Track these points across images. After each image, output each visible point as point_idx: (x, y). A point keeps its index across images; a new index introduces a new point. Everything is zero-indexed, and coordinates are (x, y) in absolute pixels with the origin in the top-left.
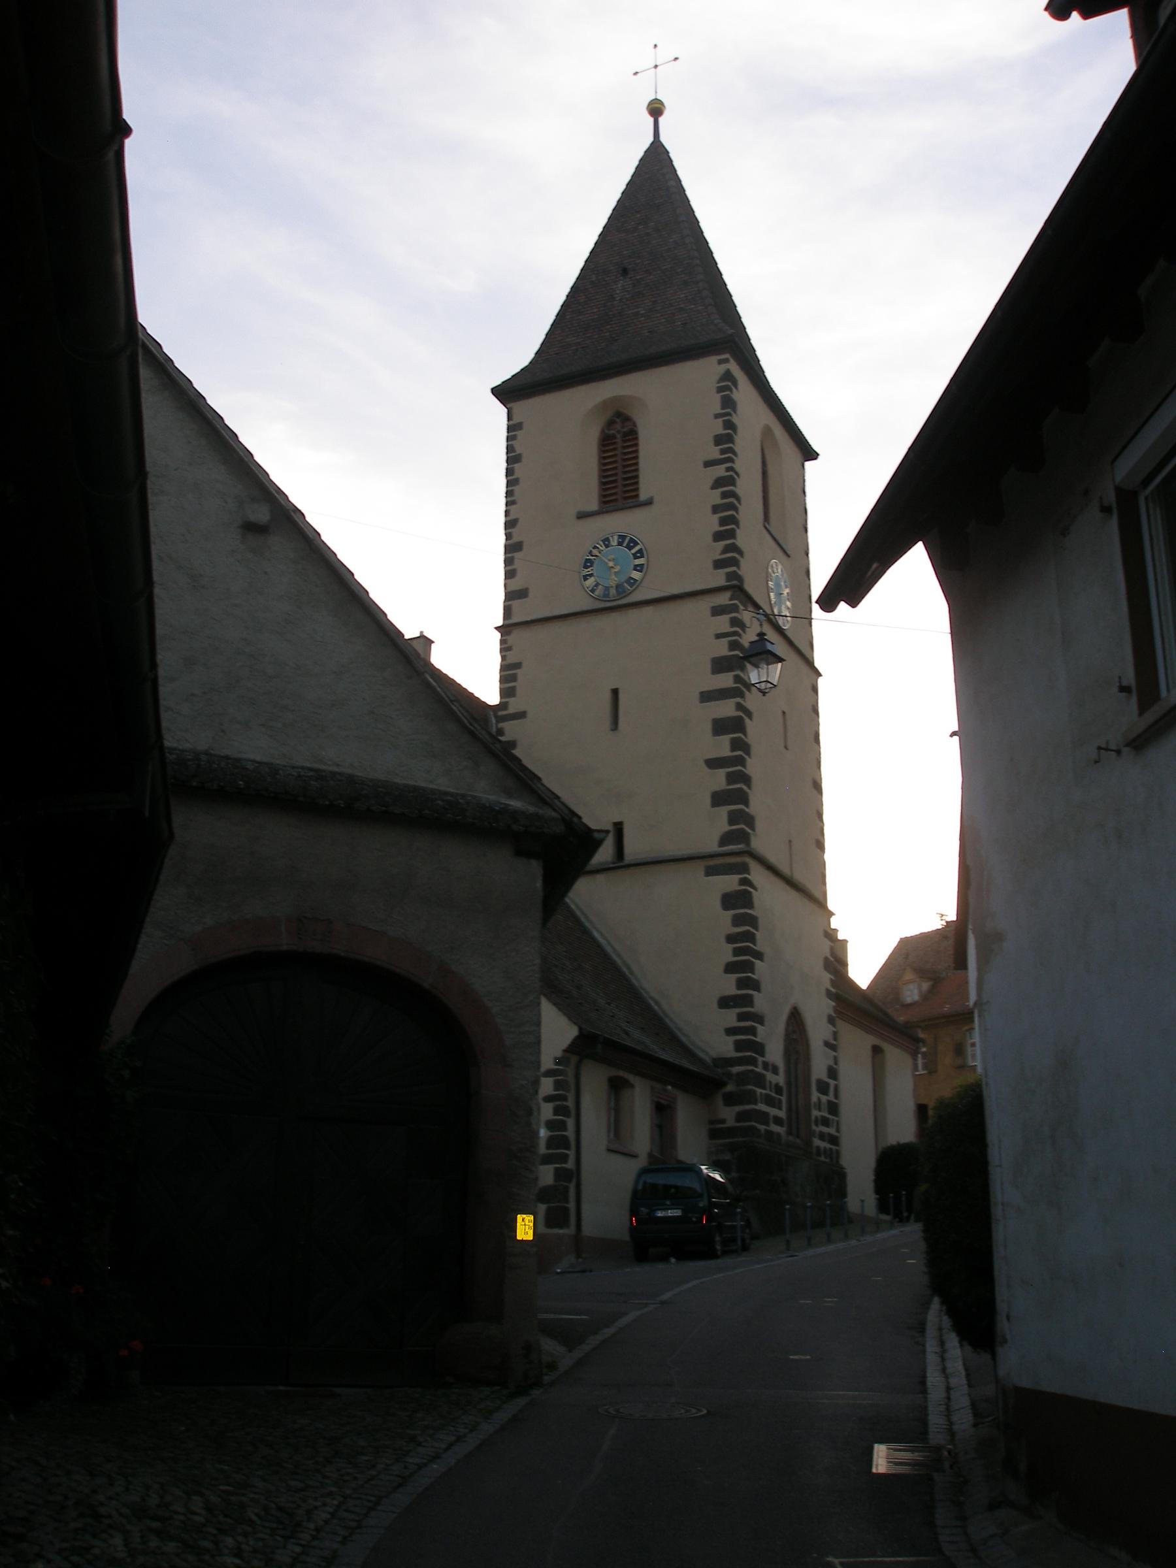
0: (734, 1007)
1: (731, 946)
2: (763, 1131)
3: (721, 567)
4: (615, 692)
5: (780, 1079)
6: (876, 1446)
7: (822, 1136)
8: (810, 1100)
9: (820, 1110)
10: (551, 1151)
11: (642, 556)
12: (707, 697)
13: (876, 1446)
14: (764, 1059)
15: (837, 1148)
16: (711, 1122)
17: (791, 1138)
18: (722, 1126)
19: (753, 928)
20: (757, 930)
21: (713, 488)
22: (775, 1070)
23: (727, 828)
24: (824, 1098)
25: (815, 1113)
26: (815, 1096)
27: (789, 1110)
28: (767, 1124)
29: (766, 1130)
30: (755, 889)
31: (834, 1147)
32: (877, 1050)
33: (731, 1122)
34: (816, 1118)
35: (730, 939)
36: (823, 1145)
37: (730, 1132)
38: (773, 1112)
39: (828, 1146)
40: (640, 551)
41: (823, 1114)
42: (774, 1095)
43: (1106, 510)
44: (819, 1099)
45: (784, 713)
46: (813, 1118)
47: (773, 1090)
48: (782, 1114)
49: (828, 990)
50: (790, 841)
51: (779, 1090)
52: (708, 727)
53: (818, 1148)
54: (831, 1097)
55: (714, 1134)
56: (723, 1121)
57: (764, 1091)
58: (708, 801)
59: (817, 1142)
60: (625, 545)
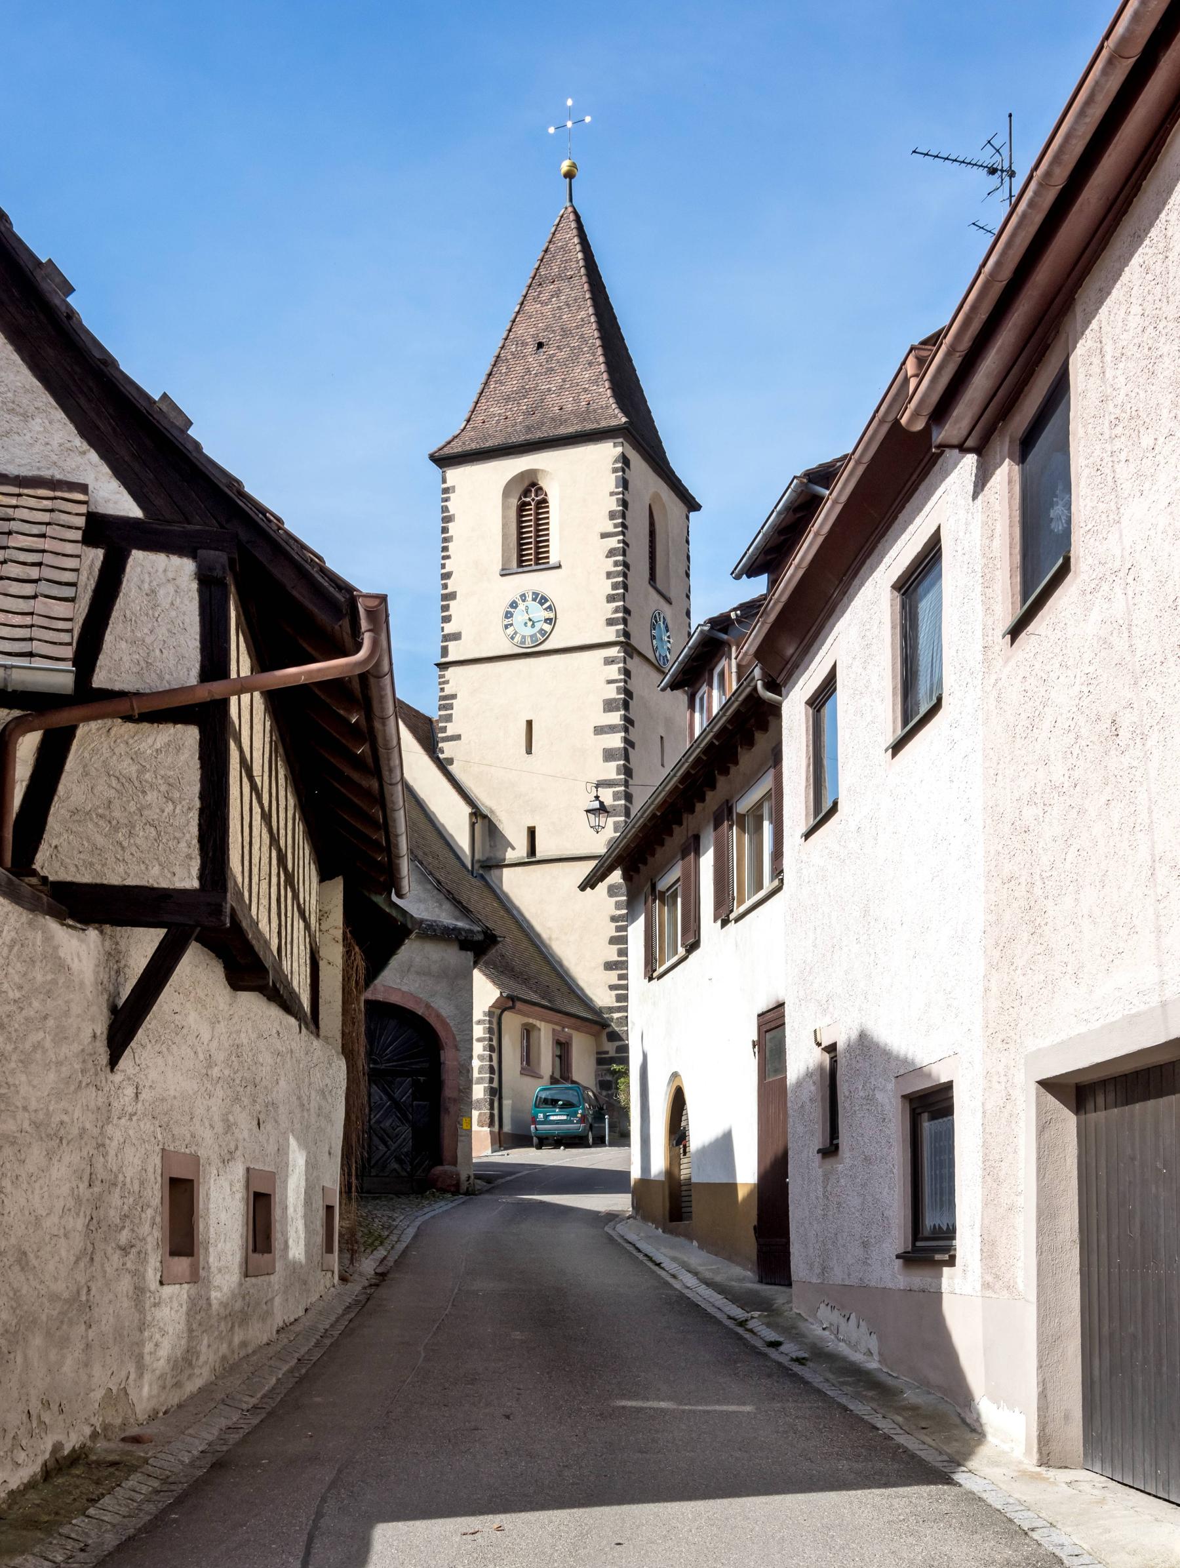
0: (616, 969)
4: (529, 723)
12: (600, 730)
16: (598, 1053)
21: (607, 557)
33: (612, 1053)
45: (662, 738)
52: (600, 756)
56: (607, 1053)
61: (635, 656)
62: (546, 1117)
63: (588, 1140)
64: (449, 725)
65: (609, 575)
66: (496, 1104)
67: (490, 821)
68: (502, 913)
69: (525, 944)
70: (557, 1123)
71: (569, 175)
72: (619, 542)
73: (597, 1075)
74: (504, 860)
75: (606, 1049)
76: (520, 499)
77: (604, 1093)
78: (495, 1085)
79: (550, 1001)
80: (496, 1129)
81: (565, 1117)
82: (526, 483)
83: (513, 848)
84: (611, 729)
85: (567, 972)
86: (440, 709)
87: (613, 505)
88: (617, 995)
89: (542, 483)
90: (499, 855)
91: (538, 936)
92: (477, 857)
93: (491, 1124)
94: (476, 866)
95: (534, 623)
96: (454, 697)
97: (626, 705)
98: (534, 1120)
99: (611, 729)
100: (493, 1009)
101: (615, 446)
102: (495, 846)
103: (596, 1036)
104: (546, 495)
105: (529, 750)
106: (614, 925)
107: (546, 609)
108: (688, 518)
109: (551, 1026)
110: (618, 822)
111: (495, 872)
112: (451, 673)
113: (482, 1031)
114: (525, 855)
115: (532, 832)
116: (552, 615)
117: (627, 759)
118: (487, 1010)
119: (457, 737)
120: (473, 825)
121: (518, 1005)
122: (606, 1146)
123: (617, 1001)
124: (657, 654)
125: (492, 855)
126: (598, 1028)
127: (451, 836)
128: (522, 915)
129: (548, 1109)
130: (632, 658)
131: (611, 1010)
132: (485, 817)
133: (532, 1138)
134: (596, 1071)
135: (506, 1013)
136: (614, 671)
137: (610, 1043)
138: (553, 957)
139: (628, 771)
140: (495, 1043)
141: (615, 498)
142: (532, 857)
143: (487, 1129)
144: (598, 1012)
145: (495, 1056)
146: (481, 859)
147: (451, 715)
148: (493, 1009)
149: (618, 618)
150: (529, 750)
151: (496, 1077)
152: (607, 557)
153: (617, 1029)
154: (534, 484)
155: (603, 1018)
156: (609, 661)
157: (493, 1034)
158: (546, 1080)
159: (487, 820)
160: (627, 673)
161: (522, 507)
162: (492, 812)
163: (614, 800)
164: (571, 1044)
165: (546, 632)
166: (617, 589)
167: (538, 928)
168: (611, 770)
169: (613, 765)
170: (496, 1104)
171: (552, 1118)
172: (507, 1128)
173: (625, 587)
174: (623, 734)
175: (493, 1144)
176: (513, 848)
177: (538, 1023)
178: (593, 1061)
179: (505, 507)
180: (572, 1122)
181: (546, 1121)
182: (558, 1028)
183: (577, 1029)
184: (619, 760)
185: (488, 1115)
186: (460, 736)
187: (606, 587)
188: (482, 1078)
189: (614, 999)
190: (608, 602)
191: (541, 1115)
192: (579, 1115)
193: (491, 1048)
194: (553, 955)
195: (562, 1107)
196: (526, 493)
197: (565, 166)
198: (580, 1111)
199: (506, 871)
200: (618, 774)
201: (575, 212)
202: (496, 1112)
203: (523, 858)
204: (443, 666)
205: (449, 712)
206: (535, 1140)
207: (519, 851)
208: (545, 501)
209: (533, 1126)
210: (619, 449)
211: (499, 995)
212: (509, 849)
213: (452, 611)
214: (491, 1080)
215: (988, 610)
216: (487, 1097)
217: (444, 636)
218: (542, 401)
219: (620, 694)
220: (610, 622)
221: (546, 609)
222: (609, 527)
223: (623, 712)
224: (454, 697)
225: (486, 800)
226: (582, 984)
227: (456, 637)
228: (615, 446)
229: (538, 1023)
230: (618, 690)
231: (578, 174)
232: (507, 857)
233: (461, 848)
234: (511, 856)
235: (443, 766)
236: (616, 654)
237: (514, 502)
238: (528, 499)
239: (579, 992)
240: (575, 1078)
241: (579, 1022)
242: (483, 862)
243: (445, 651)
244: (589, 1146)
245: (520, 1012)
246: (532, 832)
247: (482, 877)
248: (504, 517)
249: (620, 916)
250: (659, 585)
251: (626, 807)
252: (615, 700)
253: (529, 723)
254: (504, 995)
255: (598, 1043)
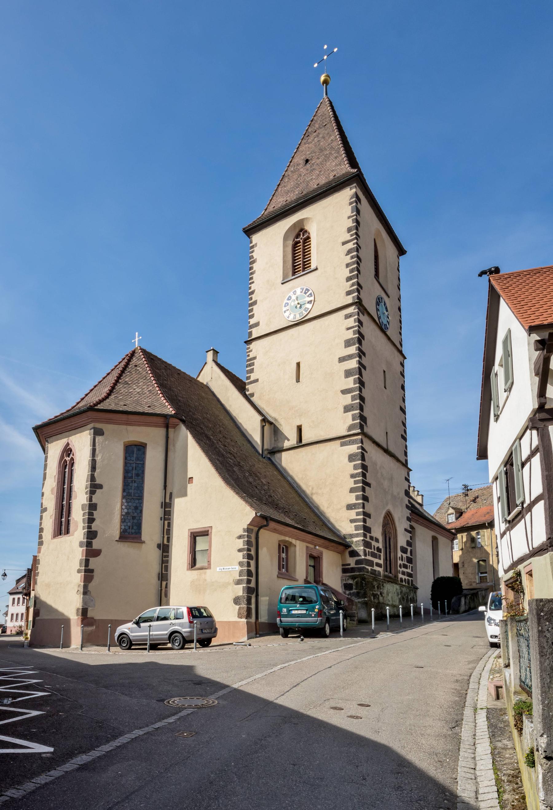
0: (355, 509)
1: (353, 480)
2: (370, 570)
3: (350, 294)
4: (298, 364)
5: (380, 545)
6: (53, 749)
7: (403, 573)
8: (397, 555)
9: (402, 560)
10: (241, 578)
11: (312, 296)
12: (342, 360)
13: (53, 749)
14: (370, 535)
15: (412, 579)
16: (343, 565)
17: (386, 573)
18: (347, 567)
19: (366, 471)
20: (367, 472)
21: (346, 255)
22: (377, 540)
23: (238, 578)
24: (405, 556)
25: (400, 562)
26: (400, 554)
27: (386, 560)
28: (373, 566)
29: (371, 569)
30: (367, 452)
31: (410, 579)
32: (435, 539)
33: (353, 565)
34: (400, 564)
35: (352, 476)
36: (404, 577)
37: (353, 570)
38: (376, 560)
39: (407, 578)
40: (311, 294)
41: (404, 562)
42: (376, 552)
43: (478, 534)
44: (402, 556)
45: (384, 372)
46: (399, 564)
47: (376, 550)
48: (381, 562)
49: (406, 505)
50: (387, 433)
51: (379, 550)
52: (343, 374)
53: (401, 579)
54: (409, 555)
55: (345, 571)
56: (349, 565)
57: (370, 550)
58: (342, 410)
59: (400, 576)
60: (303, 292)
61: (365, 314)
62: (289, 611)
63: (325, 631)
64: (252, 375)
65: (348, 265)
66: (253, 600)
67: (275, 426)
68: (279, 477)
69: (294, 495)
70: (298, 617)
71: (326, 82)
72: (354, 244)
73: (342, 580)
74: (283, 447)
75: (348, 562)
76: (294, 240)
77: (348, 592)
78: (253, 585)
79: (303, 526)
80: (253, 619)
81: (304, 612)
82: (297, 231)
83: (288, 440)
84: (350, 357)
85: (322, 513)
86: (247, 367)
87: (351, 223)
88: (355, 526)
89: (306, 228)
90: (280, 445)
91: (304, 492)
92: (266, 447)
93: (248, 616)
94: (266, 452)
95: (301, 305)
96: (255, 358)
97: (360, 342)
98: (279, 614)
99: (350, 357)
100: (251, 527)
101: (351, 190)
102: (278, 440)
103: (342, 553)
104: (309, 234)
105: (298, 380)
106: (352, 480)
107: (308, 296)
108: (398, 258)
109: (305, 544)
110: (355, 414)
111: (277, 455)
112: (253, 346)
113: (242, 544)
114: (295, 443)
115: (299, 429)
116: (312, 298)
117: (360, 374)
118: (246, 527)
119: (256, 381)
120: (263, 427)
121: (272, 524)
122: (340, 637)
123: (356, 530)
124: (380, 320)
125: (276, 445)
126: (341, 548)
127: (251, 435)
128: (293, 479)
129: (292, 606)
130: (364, 315)
131: (352, 536)
132: (271, 423)
133: (279, 628)
134: (342, 577)
135: (262, 530)
136: (351, 322)
137: (351, 558)
138: (313, 504)
139: (361, 383)
140: (253, 553)
141: (351, 219)
142: (300, 444)
143: (244, 620)
144: (344, 538)
145: (253, 563)
146: (269, 448)
147: (253, 369)
148: (251, 527)
149: (353, 289)
150: (298, 380)
151: (253, 579)
152: (346, 255)
153: (356, 549)
154: (302, 230)
155: (346, 542)
156: (347, 317)
157: (252, 546)
158: (301, 583)
159: (273, 425)
160: (360, 322)
161: (295, 245)
162: (276, 420)
163: (352, 401)
164: (322, 558)
165: (308, 309)
166: (353, 272)
167: (304, 487)
168: (350, 383)
169: (351, 379)
170: (253, 600)
171: (293, 612)
172: (264, 618)
173: (359, 271)
174: (358, 359)
175: (249, 632)
176: (288, 440)
177: (294, 541)
178: (339, 570)
179: (285, 246)
180: (310, 616)
181: (289, 615)
182: (312, 546)
183: (327, 548)
184: (355, 375)
185: (245, 609)
186: (258, 379)
187: (346, 273)
188: (241, 580)
189: (354, 529)
190: (347, 281)
191: (285, 610)
192: (316, 610)
193: (249, 557)
194: (313, 503)
195: (301, 603)
196: (298, 236)
197: (322, 78)
198: (317, 607)
199: (284, 454)
200: (355, 384)
201: (330, 101)
202: (253, 606)
203: (294, 444)
204: (248, 342)
205: (252, 367)
206: (281, 630)
207: (292, 440)
208: (309, 238)
209: (278, 619)
210: (354, 190)
211: (254, 515)
212: (286, 441)
213: (255, 312)
214: (249, 582)
215: (327, 648)
216: (245, 595)
217: (250, 326)
218: (307, 185)
219: (356, 334)
220: (348, 293)
221: (308, 296)
222: (348, 237)
223: (357, 345)
224: (255, 358)
225: (272, 413)
226: (332, 520)
227: (257, 324)
228: (351, 190)
229: (294, 541)
230: (354, 333)
231: (331, 82)
232: (285, 446)
233: (256, 442)
234: (287, 444)
235: (248, 398)
236: (353, 311)
237: (290, 243)
238: (298, 240)
239: (330, 526)
240: (325, 581)
241: (326, 542)
242: (270, 450)
243: (250, 334)
244: (325, 636)
245: (275, 531)
246: (299, 429)
247: (269, 459)
248: (284, 251)
249: (357, 474)
250: (381, 280)
251: (360, 404)
252: (352, 339)
253: (298, 364)
254: (258, 514)
255: (343, 559)
